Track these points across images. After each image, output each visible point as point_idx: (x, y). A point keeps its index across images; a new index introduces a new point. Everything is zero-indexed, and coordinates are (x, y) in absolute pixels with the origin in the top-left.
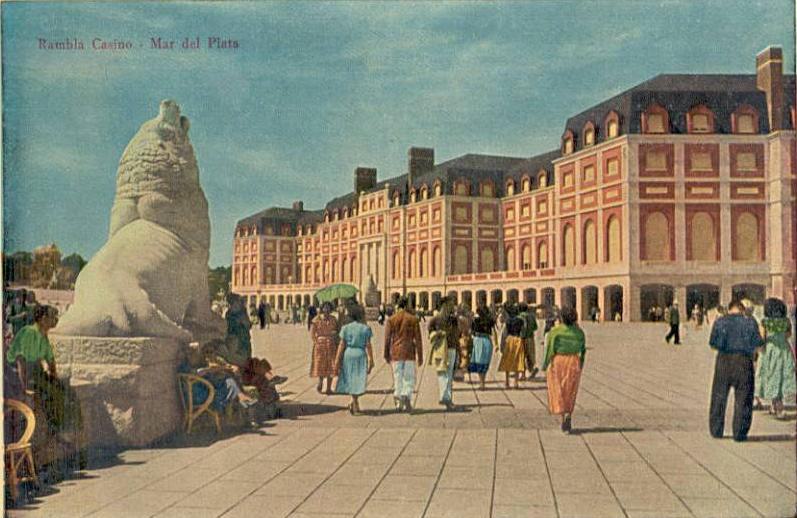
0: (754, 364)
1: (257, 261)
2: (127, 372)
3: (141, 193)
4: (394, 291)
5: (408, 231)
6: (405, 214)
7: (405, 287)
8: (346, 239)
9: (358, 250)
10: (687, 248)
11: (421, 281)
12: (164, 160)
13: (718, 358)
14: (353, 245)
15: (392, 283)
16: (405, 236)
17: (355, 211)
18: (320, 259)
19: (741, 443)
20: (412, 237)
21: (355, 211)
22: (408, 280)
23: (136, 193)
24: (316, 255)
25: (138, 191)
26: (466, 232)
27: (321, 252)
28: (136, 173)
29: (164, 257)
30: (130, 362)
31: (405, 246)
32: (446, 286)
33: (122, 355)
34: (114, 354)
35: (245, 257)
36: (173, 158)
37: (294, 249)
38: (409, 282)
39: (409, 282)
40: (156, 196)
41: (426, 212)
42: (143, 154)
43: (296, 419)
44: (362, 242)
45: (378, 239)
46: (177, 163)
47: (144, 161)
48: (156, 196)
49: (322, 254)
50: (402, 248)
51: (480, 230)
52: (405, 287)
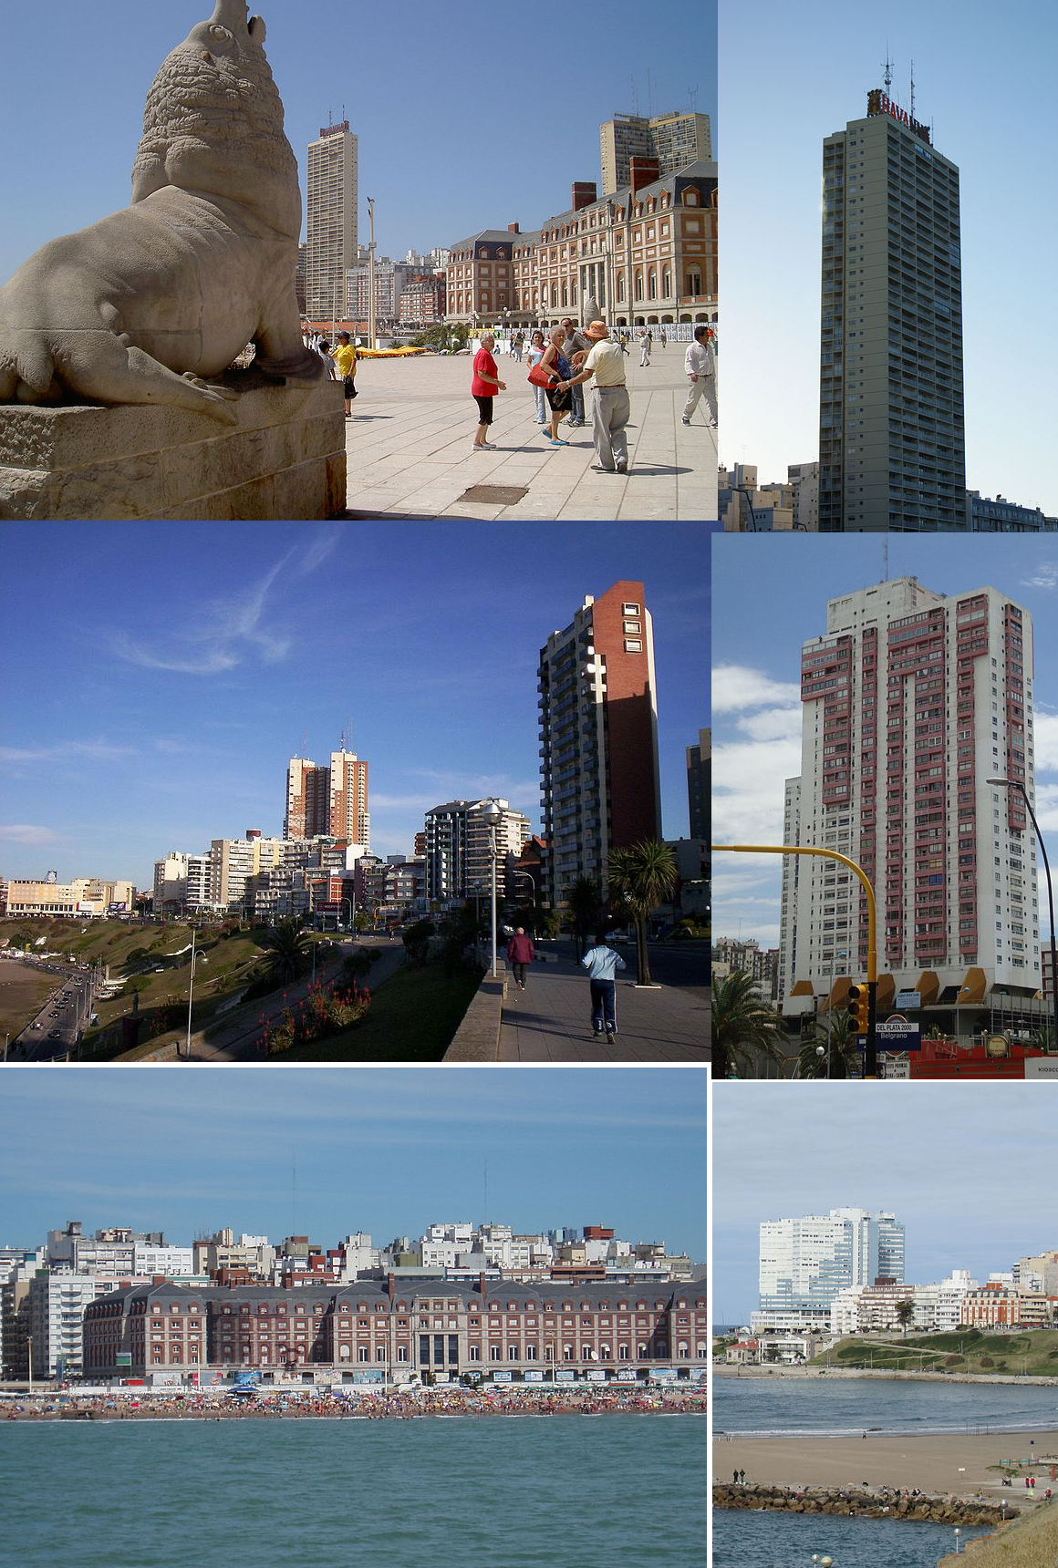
0: (190, 1041)
2: (24, 486)
4: (618, 315)
7: (631, 311)
10: (898, 373)
11: (651, 304)
12: (210, 81)
13: (704, 919)
15: (618, 306)
23: (162, 140)
26: (698, 248)
29: (185, 246)
30: (32, 464)
33: (19, 448)
38: (636, 305)
39: (636, 305)
40: (188, 142)
42: (177, 74)
46: (235, 86)
47: (176, 86)
48: (188, 142)
52: (631, 311)
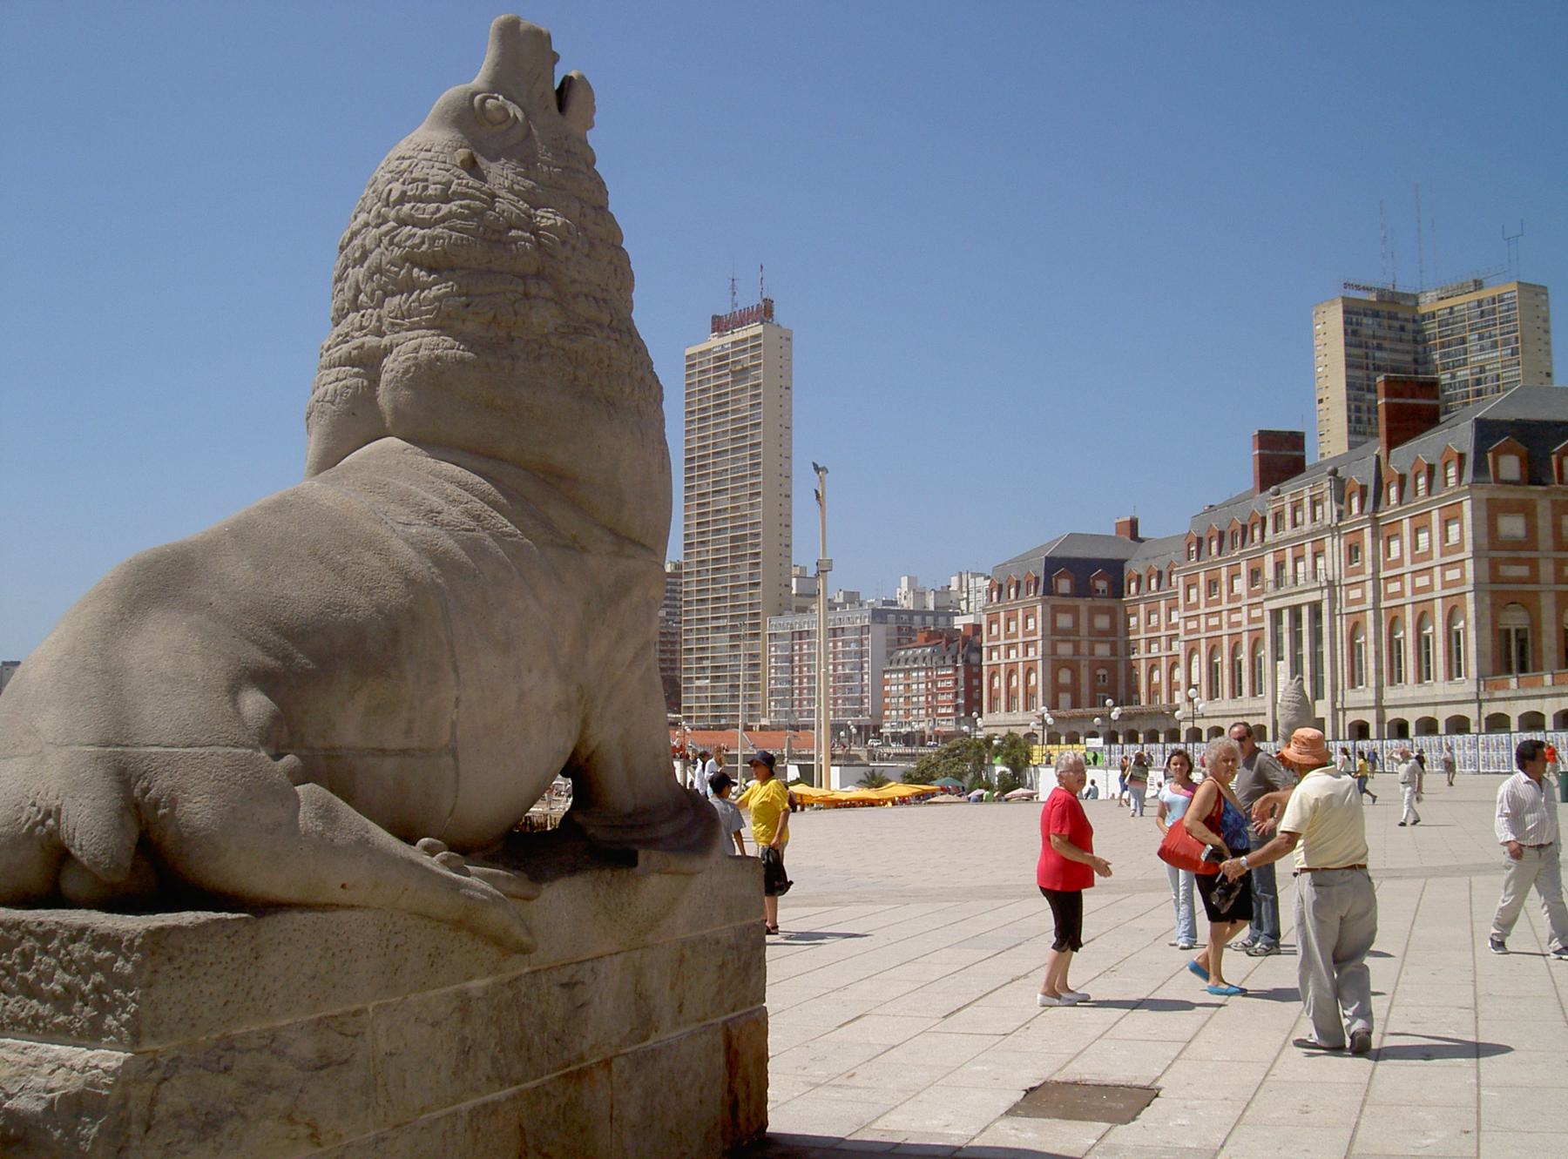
1: (1035, 653)
2: (76, 1083)
3: (386, 341)
4: (1352, 717)
5: (1383, 575)
6: (1375, 535)
7: (1380, 707)
8: (1239, 597)
9: (1267, 624)
14: (1256, 613)
15: (1351, 697)
16: (1376, 589)
17: (1257, 533)
18: (1178, 647)
19: (275, 496)
20: (1394, 587)
21: (1257, 533)
22: (1387, 690)
23: (371, 341)
24: (1172, 638)
25: (381, 334)
26: (1523, 571)
27: (1181, 631)
28: (379, 270)
31: (1376, 608)
32: (1480, 702)
33: (63, 1001)
34: (31, 991)
35: (1009, 647)
36: (507, 205)
37: (1121, 626)
38: (1390, 695)
39: (1390, 695)
41: (1427, 527)
43: (1381, 293)
44: (1275, 604)
45: (1315, 596)
46: (528, 224)
47: (402, 223)
49: (1183, 637)
50: (1370, 615)
51: (1534, 578)
